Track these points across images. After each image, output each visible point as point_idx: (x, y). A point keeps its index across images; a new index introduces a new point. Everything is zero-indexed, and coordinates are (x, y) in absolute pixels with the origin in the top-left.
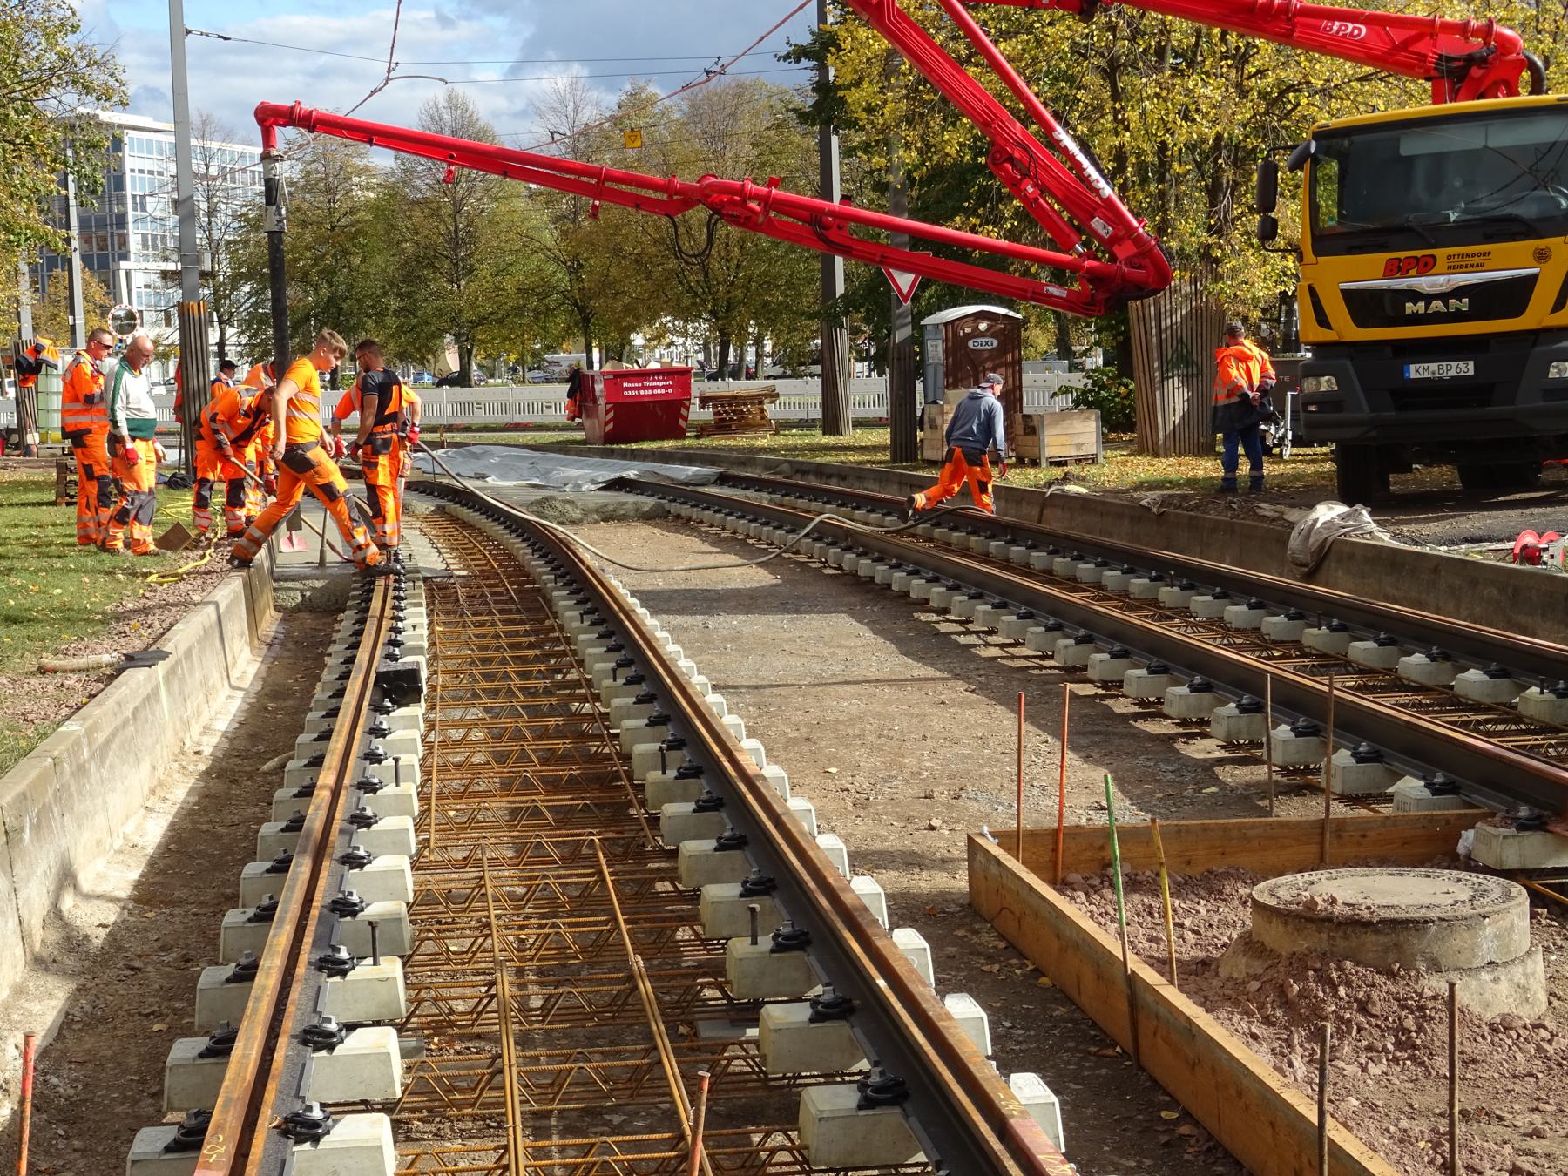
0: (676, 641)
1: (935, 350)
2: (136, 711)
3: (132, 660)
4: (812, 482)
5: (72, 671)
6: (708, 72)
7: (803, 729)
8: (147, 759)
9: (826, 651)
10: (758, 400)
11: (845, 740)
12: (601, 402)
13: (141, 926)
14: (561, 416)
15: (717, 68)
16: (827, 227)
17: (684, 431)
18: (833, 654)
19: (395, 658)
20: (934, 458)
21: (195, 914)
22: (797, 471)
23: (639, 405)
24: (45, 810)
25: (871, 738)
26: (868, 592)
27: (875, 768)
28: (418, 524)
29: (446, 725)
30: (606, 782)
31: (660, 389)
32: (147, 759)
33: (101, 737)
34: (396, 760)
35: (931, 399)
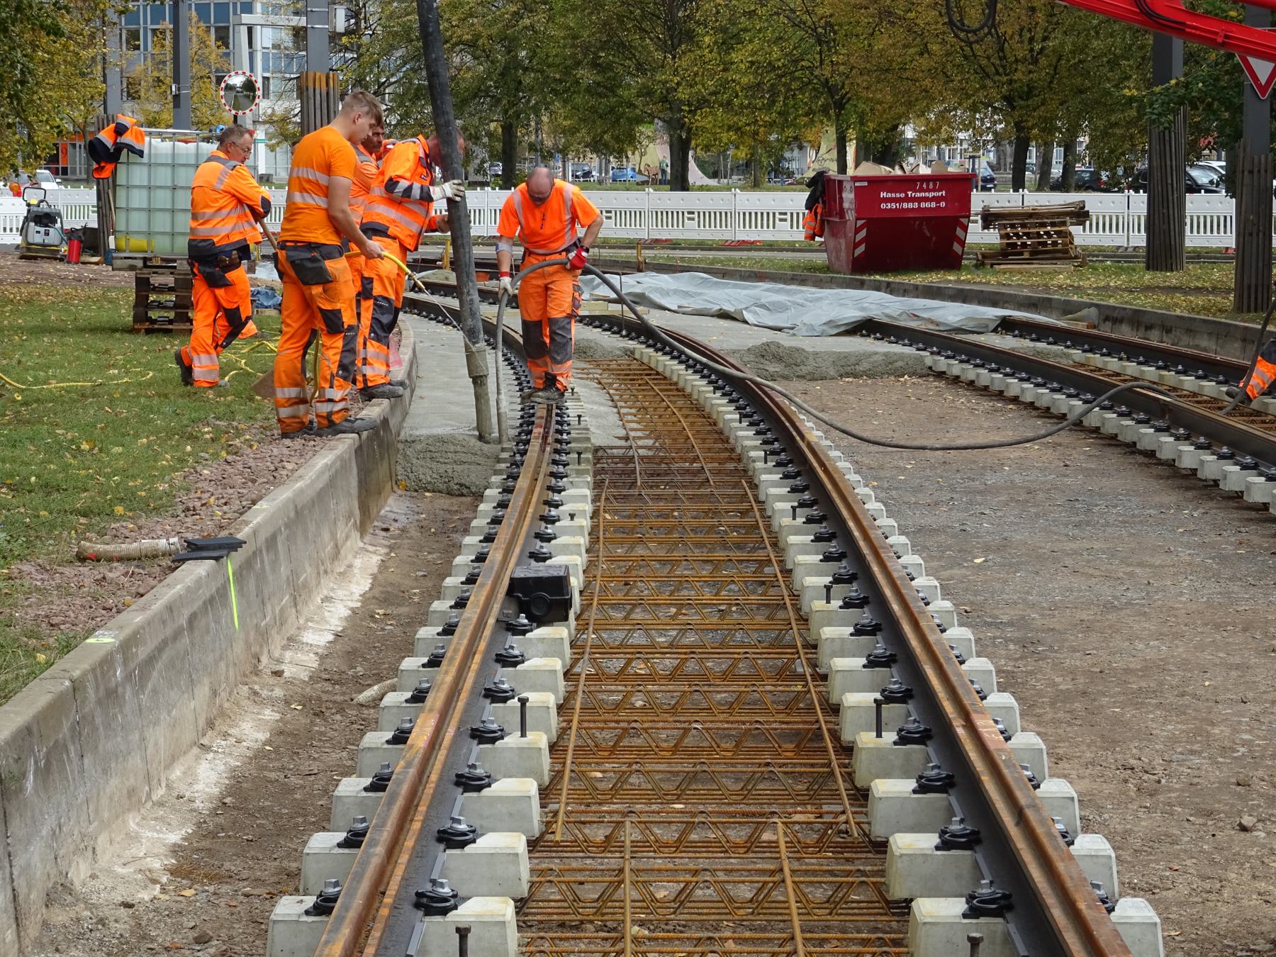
0: (917, 548)
2: (193, 618)
3: (196, 550)
4: (1126, 333)
5: (120, 559)
8: (206, 681)
10: (1059, 218)
11: (1136, 699)
12: (850, 216)
13: (175, 907)
14: (799, 235)
17: (960, 258)
19: (540, 557)
21: (247, 895)
22: (1107, 319)
23: (899, 222)
24: (58, 749)
25: (1171, 698)
26: (1188, 489)
27: (1173, 740)
28: (597, 373)
29: (600, 647)
30: (808, 741)
32: (206, 681)
33: (142, 653)
34: (523, 702)
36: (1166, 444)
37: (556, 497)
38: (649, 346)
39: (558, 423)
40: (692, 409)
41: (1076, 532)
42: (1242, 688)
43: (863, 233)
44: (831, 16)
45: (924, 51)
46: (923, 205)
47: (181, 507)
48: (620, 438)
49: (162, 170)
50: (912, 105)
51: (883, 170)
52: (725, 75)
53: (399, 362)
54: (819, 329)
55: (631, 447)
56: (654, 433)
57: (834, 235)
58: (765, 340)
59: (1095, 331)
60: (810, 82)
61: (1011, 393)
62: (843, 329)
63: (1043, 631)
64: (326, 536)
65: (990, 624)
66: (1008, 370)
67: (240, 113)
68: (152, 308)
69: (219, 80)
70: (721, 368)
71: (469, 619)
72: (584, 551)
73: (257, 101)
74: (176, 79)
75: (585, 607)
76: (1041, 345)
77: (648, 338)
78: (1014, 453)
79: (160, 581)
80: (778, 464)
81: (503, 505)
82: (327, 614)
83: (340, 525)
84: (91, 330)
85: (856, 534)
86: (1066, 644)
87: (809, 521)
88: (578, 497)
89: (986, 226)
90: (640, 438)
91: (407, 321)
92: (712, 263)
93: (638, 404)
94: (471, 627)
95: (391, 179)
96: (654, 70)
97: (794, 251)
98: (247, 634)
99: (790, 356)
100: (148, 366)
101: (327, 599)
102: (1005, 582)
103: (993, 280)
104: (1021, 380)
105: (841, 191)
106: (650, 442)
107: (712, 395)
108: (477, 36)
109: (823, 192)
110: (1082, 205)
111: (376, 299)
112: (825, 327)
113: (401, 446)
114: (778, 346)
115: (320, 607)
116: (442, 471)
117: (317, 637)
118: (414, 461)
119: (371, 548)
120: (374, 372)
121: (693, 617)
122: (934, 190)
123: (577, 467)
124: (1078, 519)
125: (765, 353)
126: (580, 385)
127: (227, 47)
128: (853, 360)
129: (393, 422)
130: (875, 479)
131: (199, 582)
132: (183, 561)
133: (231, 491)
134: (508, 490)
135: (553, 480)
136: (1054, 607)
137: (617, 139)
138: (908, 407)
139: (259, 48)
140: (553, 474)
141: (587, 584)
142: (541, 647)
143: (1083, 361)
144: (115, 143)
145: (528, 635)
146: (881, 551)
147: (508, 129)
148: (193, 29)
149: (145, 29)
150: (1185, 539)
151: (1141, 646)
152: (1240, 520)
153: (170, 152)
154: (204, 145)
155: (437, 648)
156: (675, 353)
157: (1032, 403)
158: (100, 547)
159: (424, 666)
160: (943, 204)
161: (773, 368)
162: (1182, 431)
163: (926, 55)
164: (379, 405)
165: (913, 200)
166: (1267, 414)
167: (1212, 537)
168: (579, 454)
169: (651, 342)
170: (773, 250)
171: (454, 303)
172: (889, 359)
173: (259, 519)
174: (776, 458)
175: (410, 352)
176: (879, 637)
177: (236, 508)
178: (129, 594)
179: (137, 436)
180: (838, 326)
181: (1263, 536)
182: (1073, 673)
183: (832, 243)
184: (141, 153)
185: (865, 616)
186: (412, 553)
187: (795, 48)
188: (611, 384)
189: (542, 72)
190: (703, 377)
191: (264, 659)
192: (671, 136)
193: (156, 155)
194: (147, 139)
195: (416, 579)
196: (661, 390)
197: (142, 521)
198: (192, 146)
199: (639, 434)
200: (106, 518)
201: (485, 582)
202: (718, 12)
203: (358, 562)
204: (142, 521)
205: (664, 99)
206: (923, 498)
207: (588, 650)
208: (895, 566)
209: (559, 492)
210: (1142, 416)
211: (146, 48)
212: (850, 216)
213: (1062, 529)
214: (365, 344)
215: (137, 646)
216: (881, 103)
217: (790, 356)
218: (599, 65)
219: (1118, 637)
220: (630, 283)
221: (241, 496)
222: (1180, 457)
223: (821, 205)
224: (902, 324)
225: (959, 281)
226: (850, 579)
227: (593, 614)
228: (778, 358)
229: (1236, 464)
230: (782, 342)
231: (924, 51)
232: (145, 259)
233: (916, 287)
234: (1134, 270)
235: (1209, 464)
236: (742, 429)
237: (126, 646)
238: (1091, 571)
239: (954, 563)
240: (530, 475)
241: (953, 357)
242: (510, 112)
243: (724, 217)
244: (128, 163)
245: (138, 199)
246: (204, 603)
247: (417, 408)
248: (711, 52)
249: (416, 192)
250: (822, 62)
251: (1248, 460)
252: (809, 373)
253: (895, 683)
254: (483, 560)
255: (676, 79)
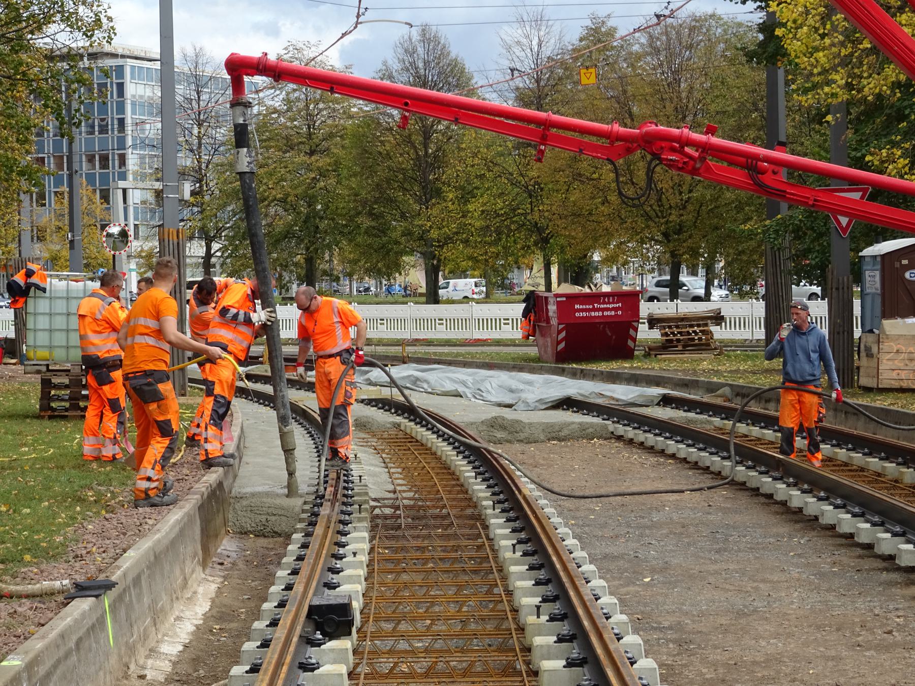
1: (873, 279)
3: (82, 590)
6: (658, 16)
7: (721, 670)
9: (749, 586)
10: (702, 320)
12: (554, 322)
14: (518, 334)
15: (667, 13)
16: (763, 172)
18: (756, 589)
20: (869, 385)
22: (737, 395)
23: (589, 326)
26: (796, 522)
28: (374, 442)
31: (610, 311)
33: (42, 670)
35: (868, 328)
36: (781, 489)
37: (344, 539)
38: (411, 421)
39: (345, 481)
40: (441, 468)
41: (717, 556)
42: (836, 675)
43: (563, 334)
44: (538, 177)
45: (605, 201)
46: (606, 313)
47: (72, 554)
48: (389, 492)
49: (59, 302)
50: (598, 239)
51: (577, 289)
52: (463, 220)
53: (231, 439)
54: (533, 405)
55: (397, 499)
56: (413, 487)
57: (543, 335)
58: (494, 414)
59: (727, 404)
60: (524, 225)
61: (670, 451)
62: (550, 405)
63: (693, 633)
64: (177, 572)
65: (655, 629)
66: (667, 434)
67: (117, 253)
68: (54, 401)
69: (103, 227)
70: (464, 439)
71: (279, 638)
72: (363, 579)
73: (129, 244)
74: (72, 230)
75: (365, 622)
76: (691, 415)
77: (410, 414)
78: (675, 496)
79: (56, 614)
80: (503, 511)
81: (305, 546)
82: (178, 630)
83: (188, 562)
84: (10, 417)
85: (558, 566)
86: (710, 643)
87: (525, 554)
88: (359, 540)
89: (651, 327)
90: (404, 491)
91: (239, 405)
92: (456, 356)
93: (403, 465)
94: (281, 645)
95: (224, 308)
96: (412, 217)
97: (515, 345)
98: (120, 649)
99: (512, 426)
100: (50, 444)
101: (178, 618)
102: (666, 595)
103: (657, 366)
104: (677, 442)
105: (547, 304)
106: (411, 494)
107: (455, 458)
108: (287, 195)
109: (534, 305)
110: (719, 312)
111: (216, 397)
112: (537, 404)
113: (232, 501)
114: (503, 419)
115: (173, 625)
116: (257, 520)
117: (171, 648)
118: (239, 512)
119: (210, 578)
120: (213, 448)
121: (440, 627)
122: (613, 303)
123: (358, 515)
124: (718, 547)
125: (494, 424)
126: (361, 452)
127: (108, 204)
128: (557, 428)
129: (226, 485)
130: (574, 518)
131: (84, 615)
132: (73, 598)
133: (108, 542)
134: (308, 535)
135: (341, 526)
136: (702, 614)
137: (388, 267)
138: (597, 462)
139: (131, 203)
140: (341, 522)
141: (366, 605)
142: (332, 655)
143: (721, 426)
144: (26, 283)
145: (323, 647)
146: (575, 579)
147: (310, 261)
148: (83, 190)
149: (50, 191)
150: (795, 560)
151: (763, 643)
152: (834, 545)
153: (65, 288)
154: (89, 283)
155: (256, 659)
156: (430, 426)
157: (685, 459)
158: (13, 588)
159: (247, 672)
160: (620, 313)
161: (500, 435)
162: (791, 480)
163: (606, 204)
164: (216, 472)
165: (599, 310)
166: (852, 465)
167: (814, 559)
168: (360, 506)
169: (412, 417)
170: (499, 345)
171: (268, 389)
172: (583, 427)
173: (127, 564)
174: (501, 505)
175: (239, 430)
176: (575, 644)
177: (111, 555)
178: (33, 623)
179: (41, 500)
180: (546, 403)
181: (851, 557)
182: (715, 665)
183: (541, 341)
184: (44, 290)
185: (565, 628)
186: (240, 581)
187: (513, 200)
188: (383, 450)
189: (333, 219)
190: (449, 444)
191: (132, 667)
192: (426, 264)
193: (55, 291)
194: (48, 280)
195: (243, 601)
196: (420, 454)
197: (43, 567)
198: (81, 284)
199: (404, 488)
200: (18, 564)
201: (291, 608)
202: (458, 176)
203: (201, 590)
204: (43, 567)
205: (421, 238)
206: (608, 533)
207: (366, 656)
208: (586, 591)
209: (346, 535)
210: (763, 469)
211: (50, 205)
212: (554, 322)
213: (707, 555)
214: (206, 428)
215: (38, 666)
216: (575, 238)
217: (512, 426)
218: (374, 214)
219: (747, 637)
220: (399, 372)
221: (115, 546)
222: (790, 499)
223: (533, 314)
224: (592, 401)
225: (632, 368)
226: (555, 599)
227: (371, 627)
228: (503, 428)
229: (830, 504)
230: (506, 416)
231: (605, 201)
232: (48, 366)
233: (602, 373)
234: (757, 357)
235: (811, 504)
236: (477, 484)
237: (30, 667)
238: (727, 587)
239: (630, 582)
240: (324, 524)
241: (628, 425)
242: (311, 249)
243: (464, 322)
244: (35, 297)
245: (43, 322)
246: (88, 630)
247: (243, 471)
248: (453, 204)
249: (241, 317)
250: (532, 210)
251: (839, 501)
252: (526, 438)
253: (586, 680)
254: (291, 587)
255: (429, 224)
